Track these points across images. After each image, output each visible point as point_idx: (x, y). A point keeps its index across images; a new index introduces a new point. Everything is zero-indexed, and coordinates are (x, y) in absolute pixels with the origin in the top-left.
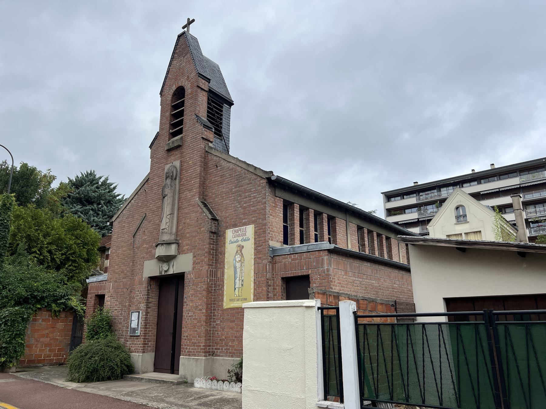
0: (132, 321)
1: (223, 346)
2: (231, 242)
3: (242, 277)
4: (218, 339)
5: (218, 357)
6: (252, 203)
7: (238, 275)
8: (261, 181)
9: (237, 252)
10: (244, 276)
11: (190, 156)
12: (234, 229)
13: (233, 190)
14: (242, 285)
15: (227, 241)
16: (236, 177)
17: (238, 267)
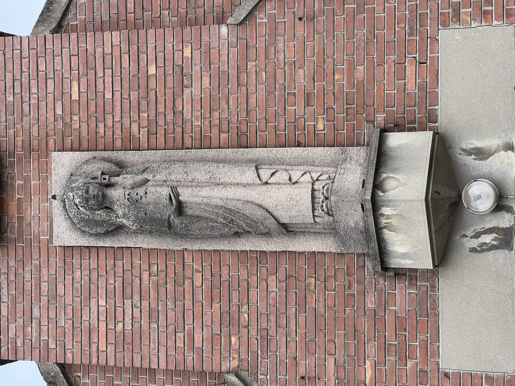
11: (50, 97)
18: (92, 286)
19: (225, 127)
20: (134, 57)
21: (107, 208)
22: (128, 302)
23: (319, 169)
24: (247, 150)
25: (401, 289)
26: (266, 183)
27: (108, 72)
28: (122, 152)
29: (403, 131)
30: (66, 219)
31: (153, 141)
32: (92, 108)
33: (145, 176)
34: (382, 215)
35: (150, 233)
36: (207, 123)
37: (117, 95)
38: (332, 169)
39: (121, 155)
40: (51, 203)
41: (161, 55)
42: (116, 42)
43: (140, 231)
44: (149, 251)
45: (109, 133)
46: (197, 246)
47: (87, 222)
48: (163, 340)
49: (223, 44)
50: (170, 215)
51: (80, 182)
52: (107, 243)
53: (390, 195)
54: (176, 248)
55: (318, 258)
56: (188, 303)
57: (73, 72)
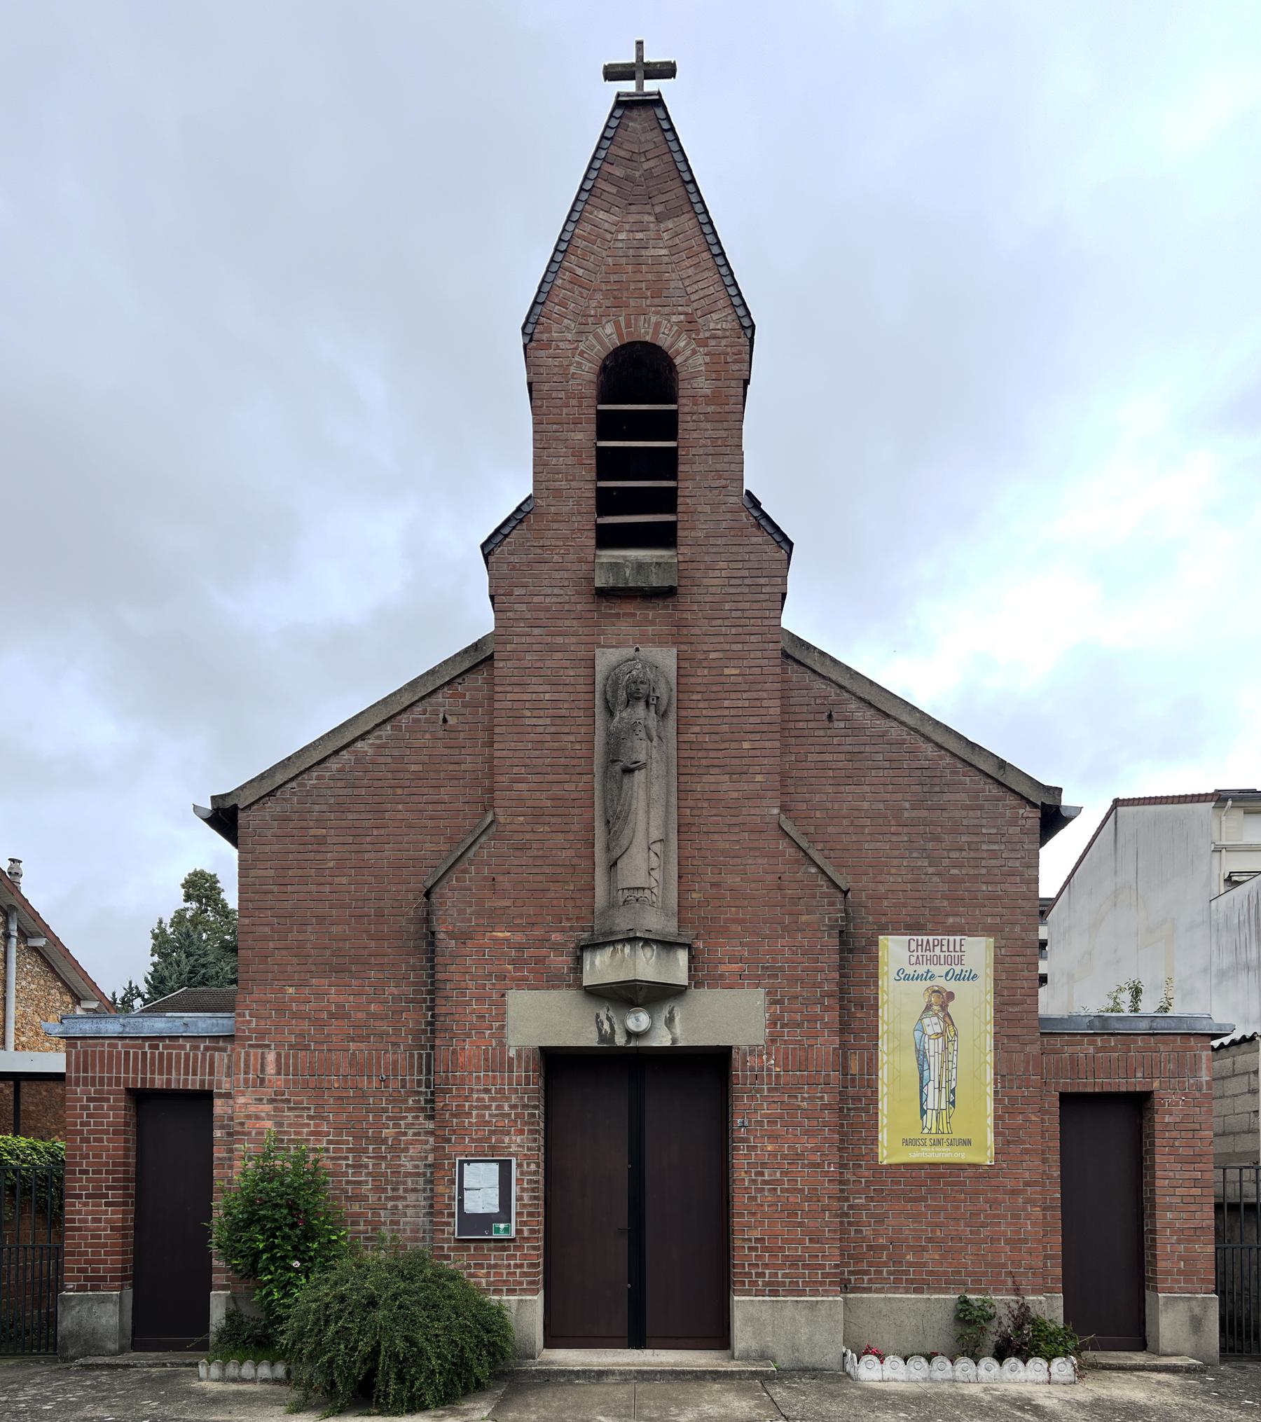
0: (466, 1193)
1: (885, 1264)
2: (902, 976)
3: (948, 1081)
4: (862, 1246)
5: (861, 1293)
6: (984, 871)
7: (933, 1073)
8: (1021, 811)
9: (928, 1008)
10: (956, 1080)
11: (727, 647)
12: (915, 938)
13: (906, 814)
14: (953, 1103)
15: (882, 969)
16: (918, 773)
17: (932, 1054)
18: (561, 687)
19: (695, 812)
20: (758, 728)
21: (628, 701)
22: (548, 721)
23: (661, 893)
24: (676, 831)
25: (567, 961)
26: (649, 849)
27: (746, 704)
28: (675, 717)
29: (689, 963)
30: (618, 661)
31: (686, 746)
32: (714, 688)
33: (656, 739)
34: (624, 946)
35: (608, 743)
36: (699, 796)
37: (726, 712)
38: (660, 905)
39: (673, 716)
40: (632, 647)
41: (758, 753)
42: (772, 711)
43: (609, 734)
44: (592, 742)
45: (692, 705)
46: (597, 786)
47: (616, 683)
48: (517, 754)
49: (764, 811)
50: (622, 761)
51: (651, 676)
52: (599, 702)
53: (640, 952)
54: (595, 767)
55: (590, 893)
56: (550, 778)
57: (747, 669)
